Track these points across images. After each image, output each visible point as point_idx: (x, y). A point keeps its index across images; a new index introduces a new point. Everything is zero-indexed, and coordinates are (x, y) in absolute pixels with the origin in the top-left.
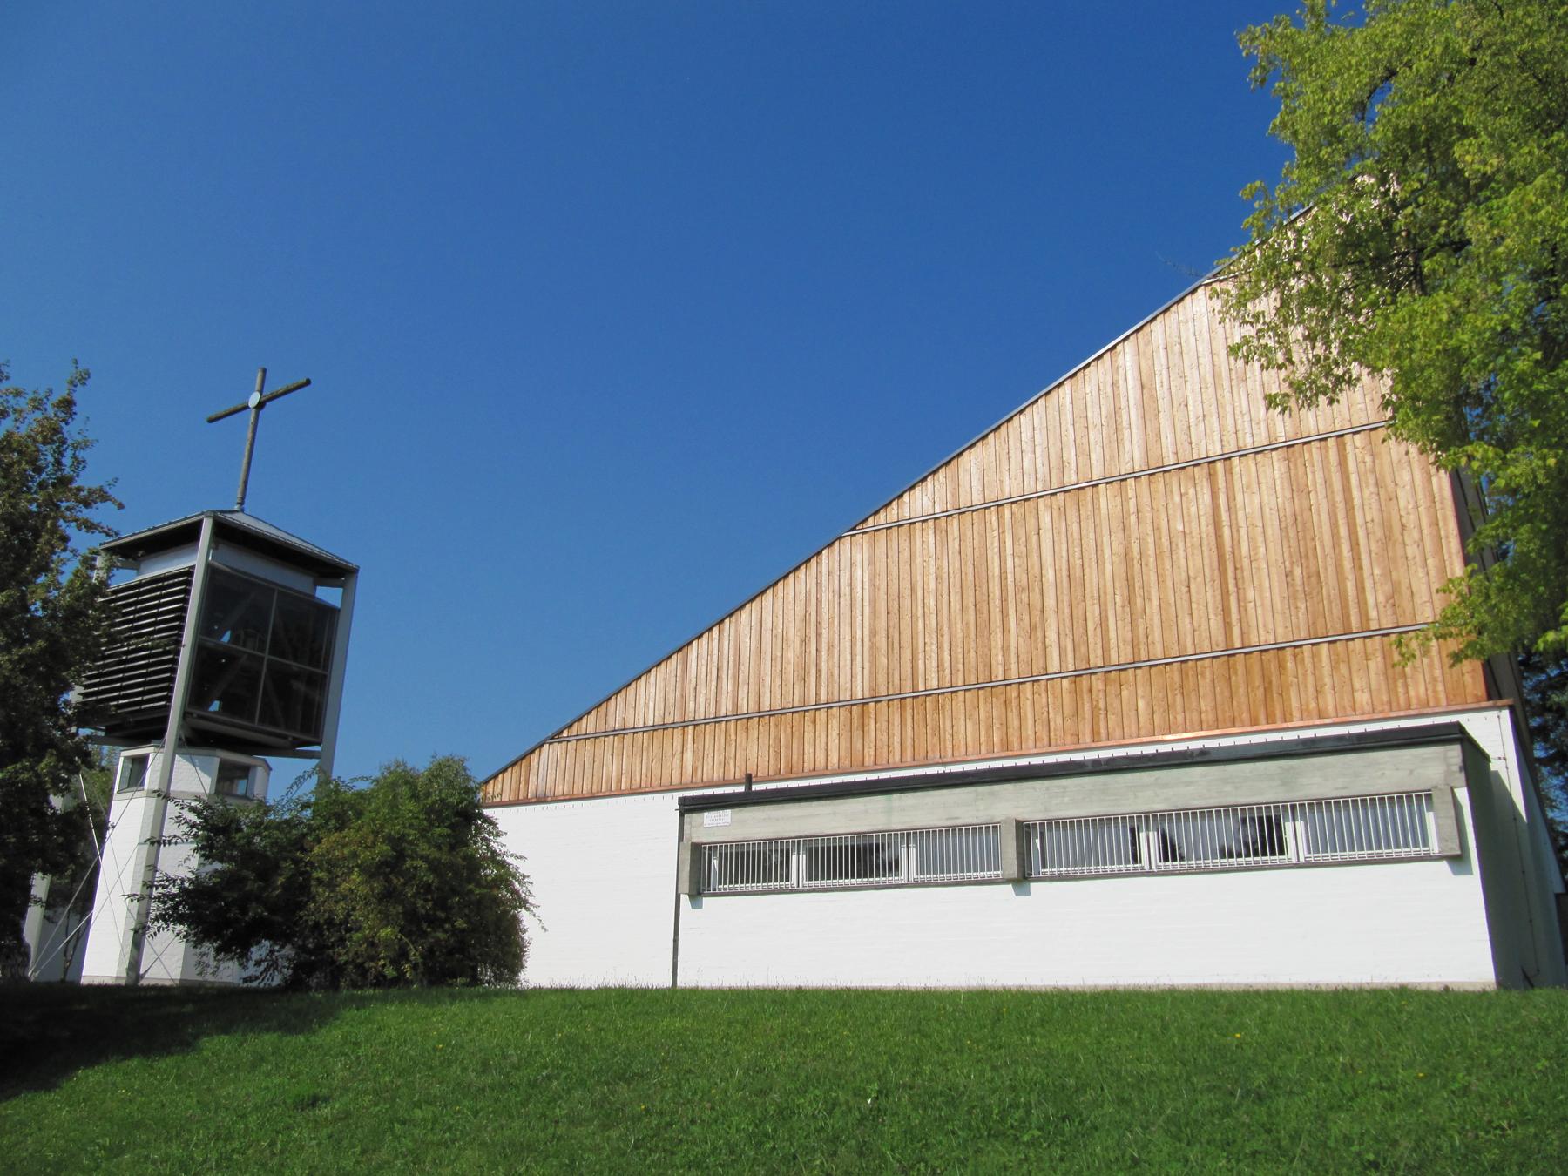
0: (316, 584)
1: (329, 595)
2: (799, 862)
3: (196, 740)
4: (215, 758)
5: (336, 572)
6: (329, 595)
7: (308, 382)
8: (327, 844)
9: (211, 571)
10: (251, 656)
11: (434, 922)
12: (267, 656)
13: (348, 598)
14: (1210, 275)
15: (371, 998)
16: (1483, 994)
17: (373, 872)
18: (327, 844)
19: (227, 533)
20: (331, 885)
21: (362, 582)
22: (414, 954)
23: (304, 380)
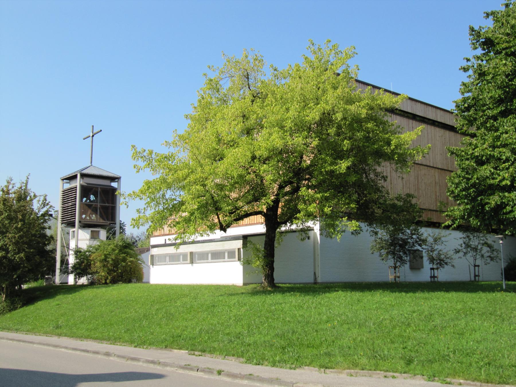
0: (111, 182)
1: (114, 185)
2: (168, 258)
3: (85, 226)
4: (89, 230)
5: (113, 179)
6: (114, 185)
7: (101, 131)
8: (93, 256)
9: (82, 187)
10: (95, 205)
11: (115, 271)
12: (99, 204)
13: (119, 185)
14: (101, 210)
15: (99, 287)
16: (240, 287)
17: (101, 261)
18: (93, 256)
19: (83, 176)
20: (94, 264)
21: (122, 180)
22: (109, 278)
23: (99, 130)
